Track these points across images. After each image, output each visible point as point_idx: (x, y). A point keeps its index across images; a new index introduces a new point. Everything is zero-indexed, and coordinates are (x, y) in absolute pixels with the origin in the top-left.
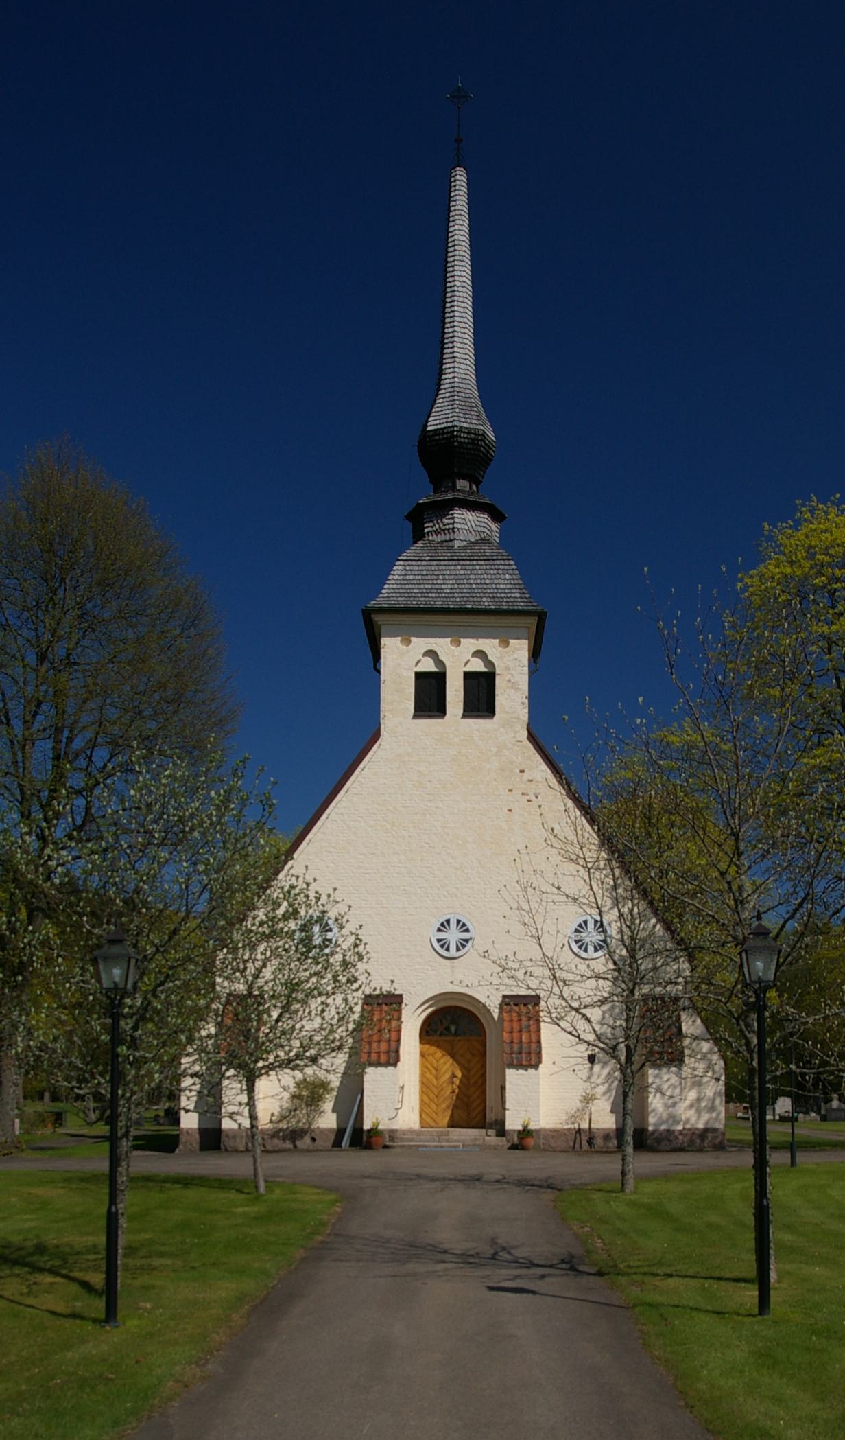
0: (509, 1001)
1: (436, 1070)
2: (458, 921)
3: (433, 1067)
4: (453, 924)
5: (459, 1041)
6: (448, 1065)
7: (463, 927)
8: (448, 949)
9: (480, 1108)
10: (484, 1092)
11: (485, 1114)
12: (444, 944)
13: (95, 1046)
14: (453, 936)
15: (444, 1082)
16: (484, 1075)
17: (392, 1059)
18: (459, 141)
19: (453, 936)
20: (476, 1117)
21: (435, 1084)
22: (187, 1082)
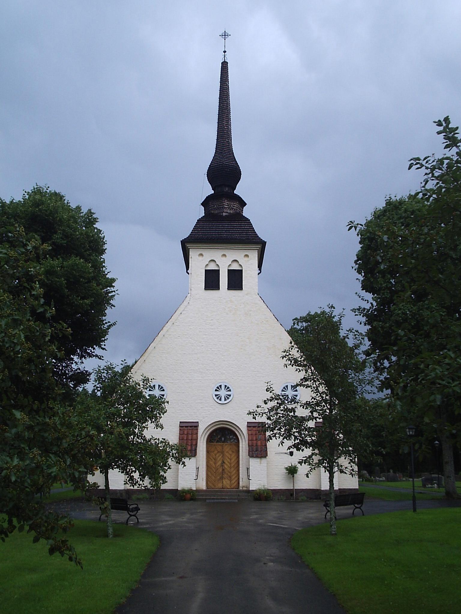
0: (379, 392)
1: (215, 459)
2: (226, 386)
3: (213, 458)
4: (223, 387)
5: (226, 445)
6: (220, 457)
7: (227, 388)
8: (220, 400)
9: (236, 479)
10: (238, 470)
11: (239, 483)
12: (218, 397)
13: (423, 605)
14: (223, 393)
15: (219, 465)
16: (238, 462)
17: (193, 453)
18: (225, 52)
19: (223, 393)
20: (234, 483)
21: (214, 467)
22: (109, 528)
